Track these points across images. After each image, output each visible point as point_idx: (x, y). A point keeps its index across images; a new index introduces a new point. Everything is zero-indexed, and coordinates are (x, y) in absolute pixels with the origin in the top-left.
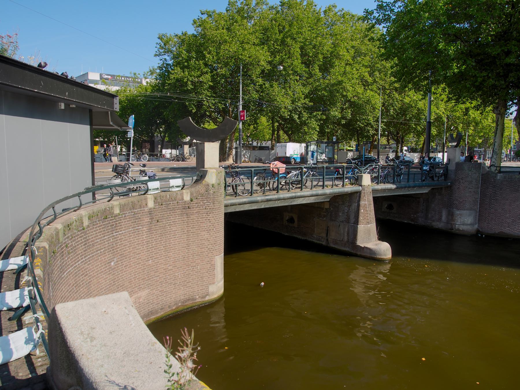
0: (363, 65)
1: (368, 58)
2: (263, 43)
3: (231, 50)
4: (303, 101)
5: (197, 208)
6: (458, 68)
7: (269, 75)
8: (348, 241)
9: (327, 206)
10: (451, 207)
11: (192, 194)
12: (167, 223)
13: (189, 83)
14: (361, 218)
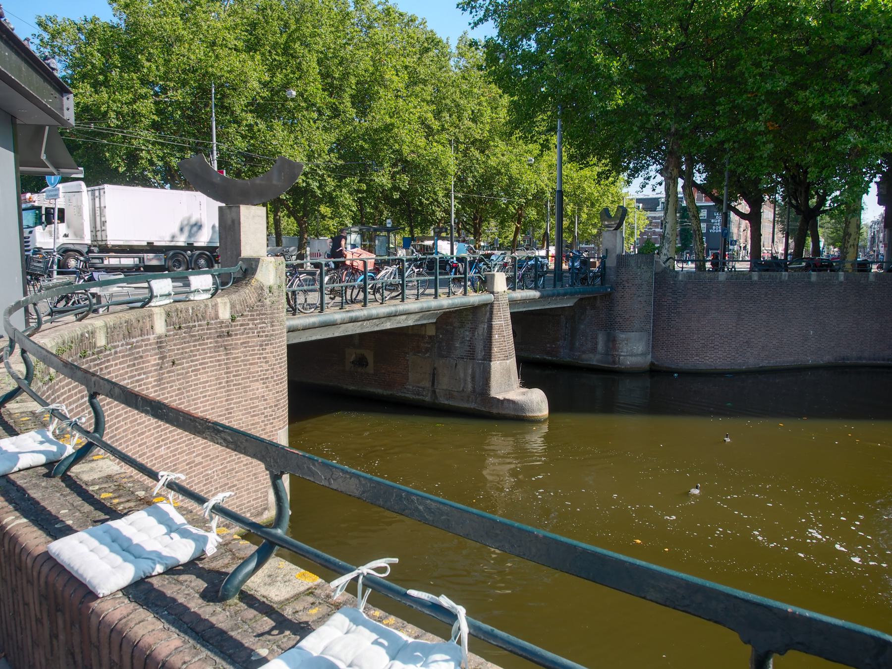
0: (423, 100)
1: (430, 88)
2: (252, 47)
3: (192, 57)
4: (327, 158)
5: (243, 334)
6: (623, 98)
7: (267, 108)
8: (474, 391)
9: (431, 332)
10: (611, 327)
11: (233, 306)
12: (191, 367)
13: (112, 115)
14: (495, 350)
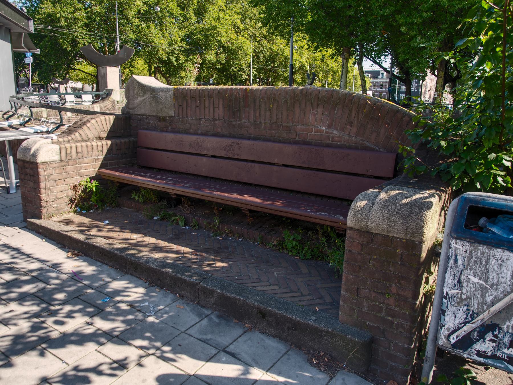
0: (235, 12)
4: (180, 44)
6: (312, 17)
13: (63, 19)
